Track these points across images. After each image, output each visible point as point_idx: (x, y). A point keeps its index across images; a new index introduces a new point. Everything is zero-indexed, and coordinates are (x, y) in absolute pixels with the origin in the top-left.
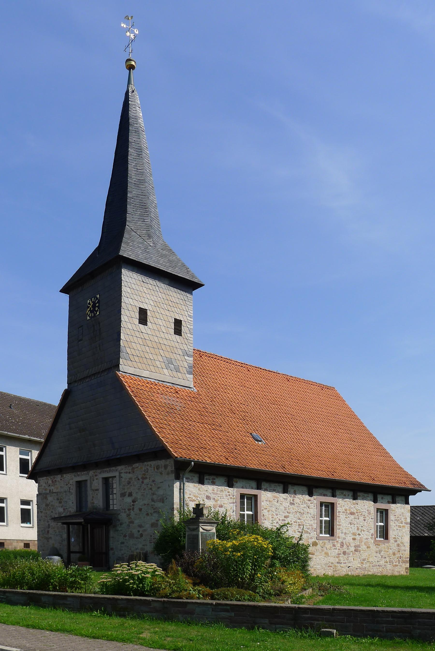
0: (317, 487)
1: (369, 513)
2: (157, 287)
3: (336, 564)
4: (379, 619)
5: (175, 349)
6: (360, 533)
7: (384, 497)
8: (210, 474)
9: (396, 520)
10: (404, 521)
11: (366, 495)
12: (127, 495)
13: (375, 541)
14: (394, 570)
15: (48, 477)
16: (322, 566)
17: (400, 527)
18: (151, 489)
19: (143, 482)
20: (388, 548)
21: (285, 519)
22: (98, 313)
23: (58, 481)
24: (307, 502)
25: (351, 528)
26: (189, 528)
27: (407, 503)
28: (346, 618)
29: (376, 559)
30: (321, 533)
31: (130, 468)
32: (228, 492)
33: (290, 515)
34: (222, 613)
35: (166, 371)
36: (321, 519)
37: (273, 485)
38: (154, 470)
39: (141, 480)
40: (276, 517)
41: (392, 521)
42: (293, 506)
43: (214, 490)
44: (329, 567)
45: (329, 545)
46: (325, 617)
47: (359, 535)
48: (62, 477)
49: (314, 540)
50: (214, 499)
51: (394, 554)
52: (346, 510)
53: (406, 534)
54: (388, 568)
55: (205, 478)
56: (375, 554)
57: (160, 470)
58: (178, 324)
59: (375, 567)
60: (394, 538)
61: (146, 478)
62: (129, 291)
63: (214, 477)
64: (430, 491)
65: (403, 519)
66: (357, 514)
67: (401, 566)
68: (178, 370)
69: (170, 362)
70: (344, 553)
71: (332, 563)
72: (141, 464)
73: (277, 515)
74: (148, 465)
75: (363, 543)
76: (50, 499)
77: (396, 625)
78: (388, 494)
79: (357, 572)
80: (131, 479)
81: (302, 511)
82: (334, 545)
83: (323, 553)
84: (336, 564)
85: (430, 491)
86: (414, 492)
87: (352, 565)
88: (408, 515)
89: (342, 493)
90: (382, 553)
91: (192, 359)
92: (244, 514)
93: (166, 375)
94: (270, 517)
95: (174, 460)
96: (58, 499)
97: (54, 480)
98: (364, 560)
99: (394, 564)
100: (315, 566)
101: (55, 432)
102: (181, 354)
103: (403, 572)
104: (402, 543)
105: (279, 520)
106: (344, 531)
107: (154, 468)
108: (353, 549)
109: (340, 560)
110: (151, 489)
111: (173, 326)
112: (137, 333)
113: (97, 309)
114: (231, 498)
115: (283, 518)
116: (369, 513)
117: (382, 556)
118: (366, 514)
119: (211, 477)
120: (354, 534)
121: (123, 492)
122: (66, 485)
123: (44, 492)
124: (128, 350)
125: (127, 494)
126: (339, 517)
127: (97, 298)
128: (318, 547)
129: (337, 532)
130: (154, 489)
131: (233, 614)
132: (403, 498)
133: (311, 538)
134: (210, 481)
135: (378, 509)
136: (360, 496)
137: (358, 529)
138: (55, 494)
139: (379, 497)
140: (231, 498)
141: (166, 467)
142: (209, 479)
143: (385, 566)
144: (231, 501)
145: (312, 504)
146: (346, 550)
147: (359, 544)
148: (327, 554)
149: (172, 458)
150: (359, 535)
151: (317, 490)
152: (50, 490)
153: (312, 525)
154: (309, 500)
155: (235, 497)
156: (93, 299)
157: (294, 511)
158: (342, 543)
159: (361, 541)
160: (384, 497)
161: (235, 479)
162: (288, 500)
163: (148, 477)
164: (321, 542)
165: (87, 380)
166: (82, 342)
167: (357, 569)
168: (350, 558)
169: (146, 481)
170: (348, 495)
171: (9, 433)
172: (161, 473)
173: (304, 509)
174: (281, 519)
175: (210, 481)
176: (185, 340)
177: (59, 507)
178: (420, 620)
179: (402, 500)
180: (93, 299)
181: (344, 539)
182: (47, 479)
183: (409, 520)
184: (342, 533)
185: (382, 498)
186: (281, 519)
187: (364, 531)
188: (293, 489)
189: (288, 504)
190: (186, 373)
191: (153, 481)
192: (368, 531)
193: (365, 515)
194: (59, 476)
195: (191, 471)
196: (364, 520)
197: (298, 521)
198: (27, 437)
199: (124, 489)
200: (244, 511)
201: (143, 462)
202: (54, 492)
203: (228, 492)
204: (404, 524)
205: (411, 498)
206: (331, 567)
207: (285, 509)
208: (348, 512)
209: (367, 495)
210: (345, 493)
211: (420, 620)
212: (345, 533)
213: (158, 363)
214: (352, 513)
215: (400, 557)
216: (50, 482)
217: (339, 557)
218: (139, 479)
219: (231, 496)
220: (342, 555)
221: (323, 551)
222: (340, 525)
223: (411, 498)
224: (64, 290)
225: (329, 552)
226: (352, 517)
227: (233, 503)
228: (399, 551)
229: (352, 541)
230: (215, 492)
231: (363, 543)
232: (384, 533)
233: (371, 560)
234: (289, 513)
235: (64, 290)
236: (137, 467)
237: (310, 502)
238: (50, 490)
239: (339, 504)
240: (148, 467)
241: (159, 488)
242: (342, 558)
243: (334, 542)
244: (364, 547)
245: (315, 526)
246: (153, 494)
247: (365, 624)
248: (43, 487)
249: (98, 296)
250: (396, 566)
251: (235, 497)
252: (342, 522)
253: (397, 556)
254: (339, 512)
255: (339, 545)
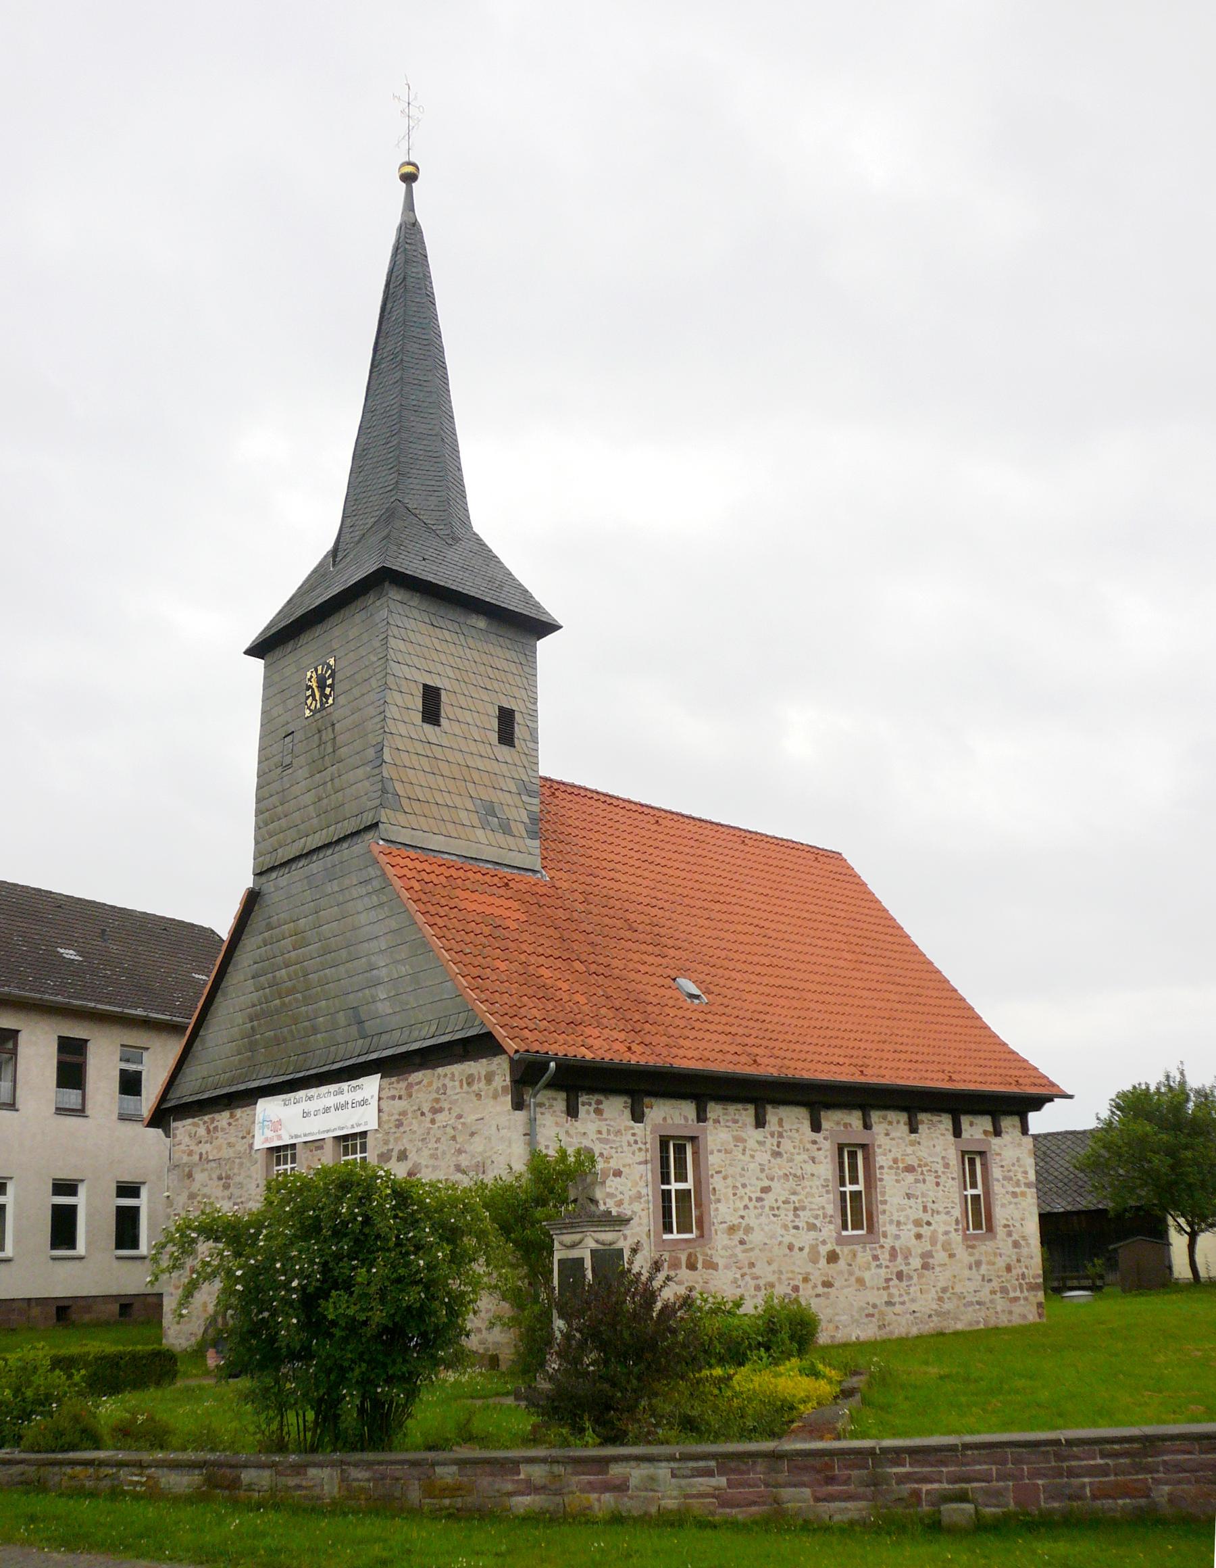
0: (829, 1106)
1: (947, 1166)
2: (462, 637)
3: (884, 1308)
4: (1073, 1463)
5: (501, 779)
7: (975, 1121)
8: (591, 1090)
9: (1005, 1178)
10: (1023, 1180)
11: (936, 1118)
12: (394, 1159)
13: (966, 1237)
14: (1011, 1312)
15: (196, 1120)
16: (852, 1316)
17: (1014, 1194)
18: (454, 1138)
19: (433, 1121)
20: (995, 1254)
21: (763, 1195)
22: (330, 701)
23: (223, 1129)
24: (809, 1146)
26: (561, 1243)
27: (1025, 1130)
28: (994, 1468)
29: (971, 1286)
30: (845, 1227)
31: (403, 1085)
32: (634, 1135)
33: (774, 1185)
34: (700, 1480)
35: (480, 833)
38: (461, 1086)
39: (429, 1116)
41: (998, 1180)
42: (779, 1160)
43: (600, 1132)
44: (867, 1316)
45: (864, 1256)
46: (944, 1469)
47: (929, 1224)
48: (232, 1116)
49: (829, 1247)
51: (1009, 1269)
52: (895, 1161)
53: (1031, 1213)
54: (999, 1308)
55: (580, 1100)
56: (967, 1272)
57: (475, 1087)
59: (970, 1309)
60: (1006, 1226)
61: (441, 1110)
62: (403, 648)
63: (602, 1098)
64: (1071, 1097)
65: (1020, 1176)
67: (1026, 1299)
68: (506, 829)
69: (490, 810)
70: (900, 1276)
71: (875, 1306)
72: (429, 1072)
73: (744, 1186)
74: (446, 1075)
75: (939, 1246)
76: (200, 1177)
77: (1112, 1478)
79: (932, 1325)
80: (404, 1113)
81: (799, 1173)
82: (876, 1258)
83: (853, 1279)
84: (884, 1308)
85: (1071, 1097)
86: (1037, 1102)
87: (917, 1309)
88: (1029, 1162)
89: (885, 1118)
90: (984, 1269)
91: (536, 801)
92: (670, 1191)
93: (484, 843)
94: (730, 1191)
95: (511, 1059)
96: (220, 1178)
97: (211, 1128)
98: (944, 1290)
99: (1012, 1295)
100: (837, 1318)
101: (219, 999)
102: (514, 790)
103: (1032, 1317)
104: (1024, 1238)
105: (750, 1199)
106: (895, 1218)
107: (461, 1081)
108: (916, 1263)
109: (890, 1295)
110: (454, 1138)
111: (495, 724)
112: (419, 746)
113: (328, 690)
114: (640, 1149)
115: (759, 1194)
116: (947, 1166)
117: (983, 1276)
118: (940, 1169)
120: (917, 1223)
121: (384, 1149)
122: (243, 1138)
123: (185, 1159)
124: (399, 788)
125: (395, 1154)
127: (329, 667)
128: (842, 1263)
129: (884, 1223)
130: (459, 1139)
131: (722, 1481)
132: (1016, 1120)
133: (824, 1242)
135: (964, 1153)
136: (922, 1122)
137: (925, 1209)
138: (213, 1164)
140: (640, 1149)
141: (489, 1078)
142: (590, 1104)
143: (992, 1301)
144: (640, 1157)
146: (903, 1268)
147: (929, 1248)
148: (861, 1281)
149: (505, 1052)
150: (929, 1224)
151: (830, 1113)
152: (201, 1154)
153: (823, 1208)
154: (814, 1142)
155: (648, 1146)
156: (320, 668)
157: (781, 1173)
158: (893, 1248)
159: (934, 1242)
160: (975, 1121)
161: (646, 1100)
162: (768, 1145)
163: (446, 1105)
164: (846, 1249)
165: (301, 865)
166: (290, 771)
167: (930, 1316)
168: (912, 1289)
169: (439, 1117)
170: (898, 1122)
171: (99, 1006)
172: (478, 1096)
173: (804, 1166)
174: (754, 1196)
175: (592, 1109)
176: (523, 757)
177: (223, 1198)
178: (1165, 1458)
179: (1014, 1126)
180: (320, 668)
181: (897, 1237)
182: (195, 1125)
183: (1032, 1177)
184: (891, 1222)
185: (971, 1124)
186: (754, 1196)
187: (938, 1213)
188: (777, 1114)
189: (768, 1156)
190: (525, 835)
191: (460, 1117)
192: (948, 1213)
194: (226, 1114)
195: (550, 1086)
196: (938, 1184)
197: (793, 1198)
198: (139, 1012)
199: (386, 1142)
200: (668, 1183)
201: (434, 1067)
202: (211, 1158)
203: (634, 1135)
204: (1023, 1189)
205: (1032, 1116)
206: (873, 1315)
207: (762, 1170)
208: (901, 1165)
209: (938, 1118)
210: (889, 1118)
211: (1165, 1458)
212: (899, 1223)
213: (463, 815)
214: (910, 1169)
215: (1023, 1275)
216: (202, 1131)
217: (888, 1287)
218: (423, 1114)
219: (640, 1145)
220: (895, 1282)
221: (851, 1274)
222: (885, 1202)
223: (1032, 1116)
224: (258, 649)
225: (867, 1276)
226: (910, 1178)
227: (646, 1162)
228: (1019, 1261)
229: (914, 1241)
230: (604, 1136)
231: (939, 1246)
232: (979, 1215)
233: (958, 1289)
234: (772, 1179)
235: (258, 649)
236: (420, 1083)
237: (815, 1147)
238: (201, 1154)
239: (879, 1146)
240: (447, 1081)
241: (472, 1134)
242: (896, 1288)
244: (940, 1256)
245: (830, 1209)
246: (460, 1152)
247: (1040, 1482)
248: (183, 1147)
249: (332, 662)
250: (1016, 1299)
251: (648, 1146)
252: (893, 1196)
253: (1014, 1272)
254: (881, 1167)
255: (887, 1256)
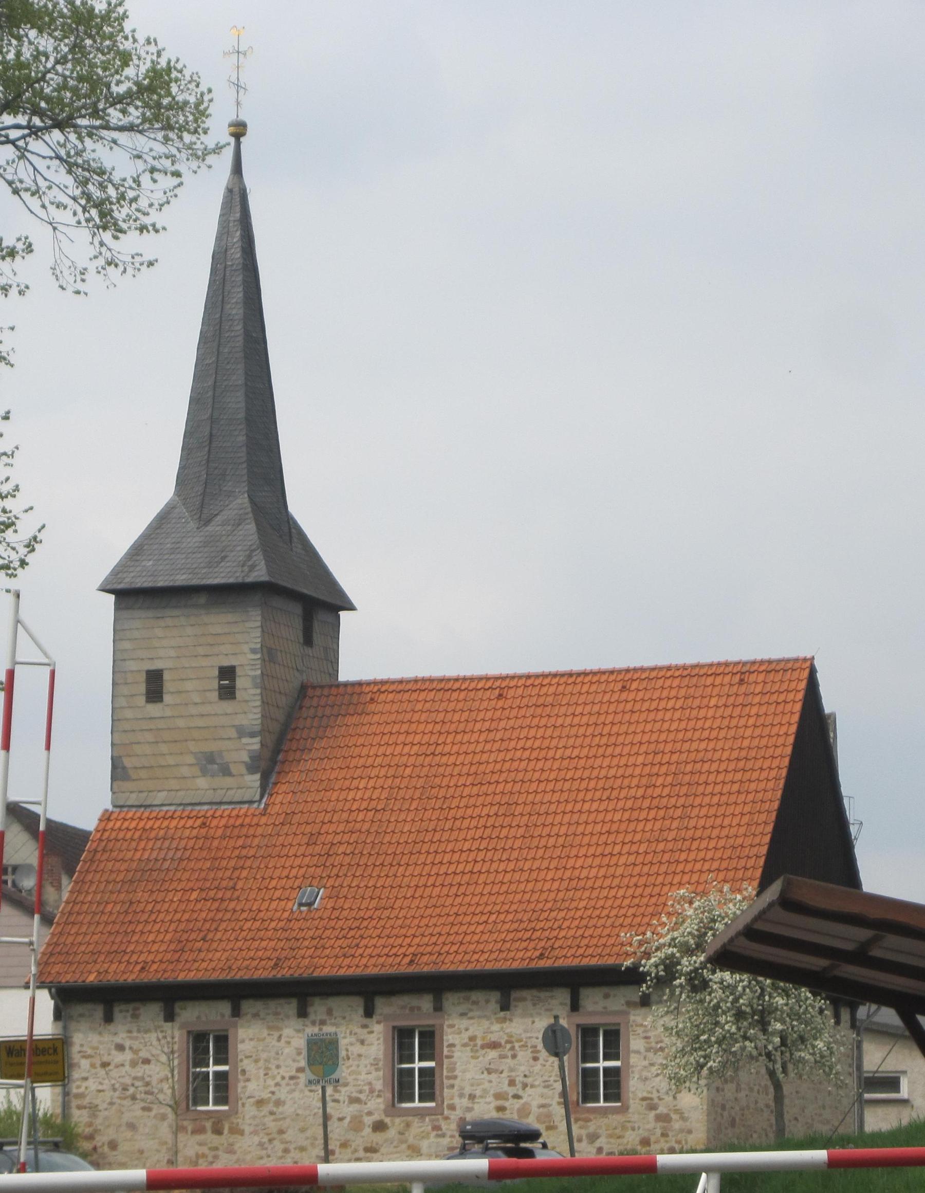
6: (520, 1093)
8: (128, 1000)
25: (490, 1082)
36: (432, 1064)
37: (273, 1004)
40: (276, 1072)
47: (517, 1097)
49: (376, 1117)
50: (131, 1048)
58: (227, 673)
66: (509, 1046)
73: (278, 1067)
78: (222, 997)
82: (437, 1128)
89: (467, 999)
106: (468, 1090)
119: (131, 1006)
126: (451, 1057)
128: (392, 1133)
134: (129, 1015)
137: (512, 1083)
139: (379, 1002)
142: (128, 1011)
145: (372, 1035)
175: (129, 1015)
184: (461, 1096)
186: (287, 1075)
193: (536, 1047)
214: (494, 1045)
226: (493, 1054)
243: (438, 1120)
254: (452, 1045)
